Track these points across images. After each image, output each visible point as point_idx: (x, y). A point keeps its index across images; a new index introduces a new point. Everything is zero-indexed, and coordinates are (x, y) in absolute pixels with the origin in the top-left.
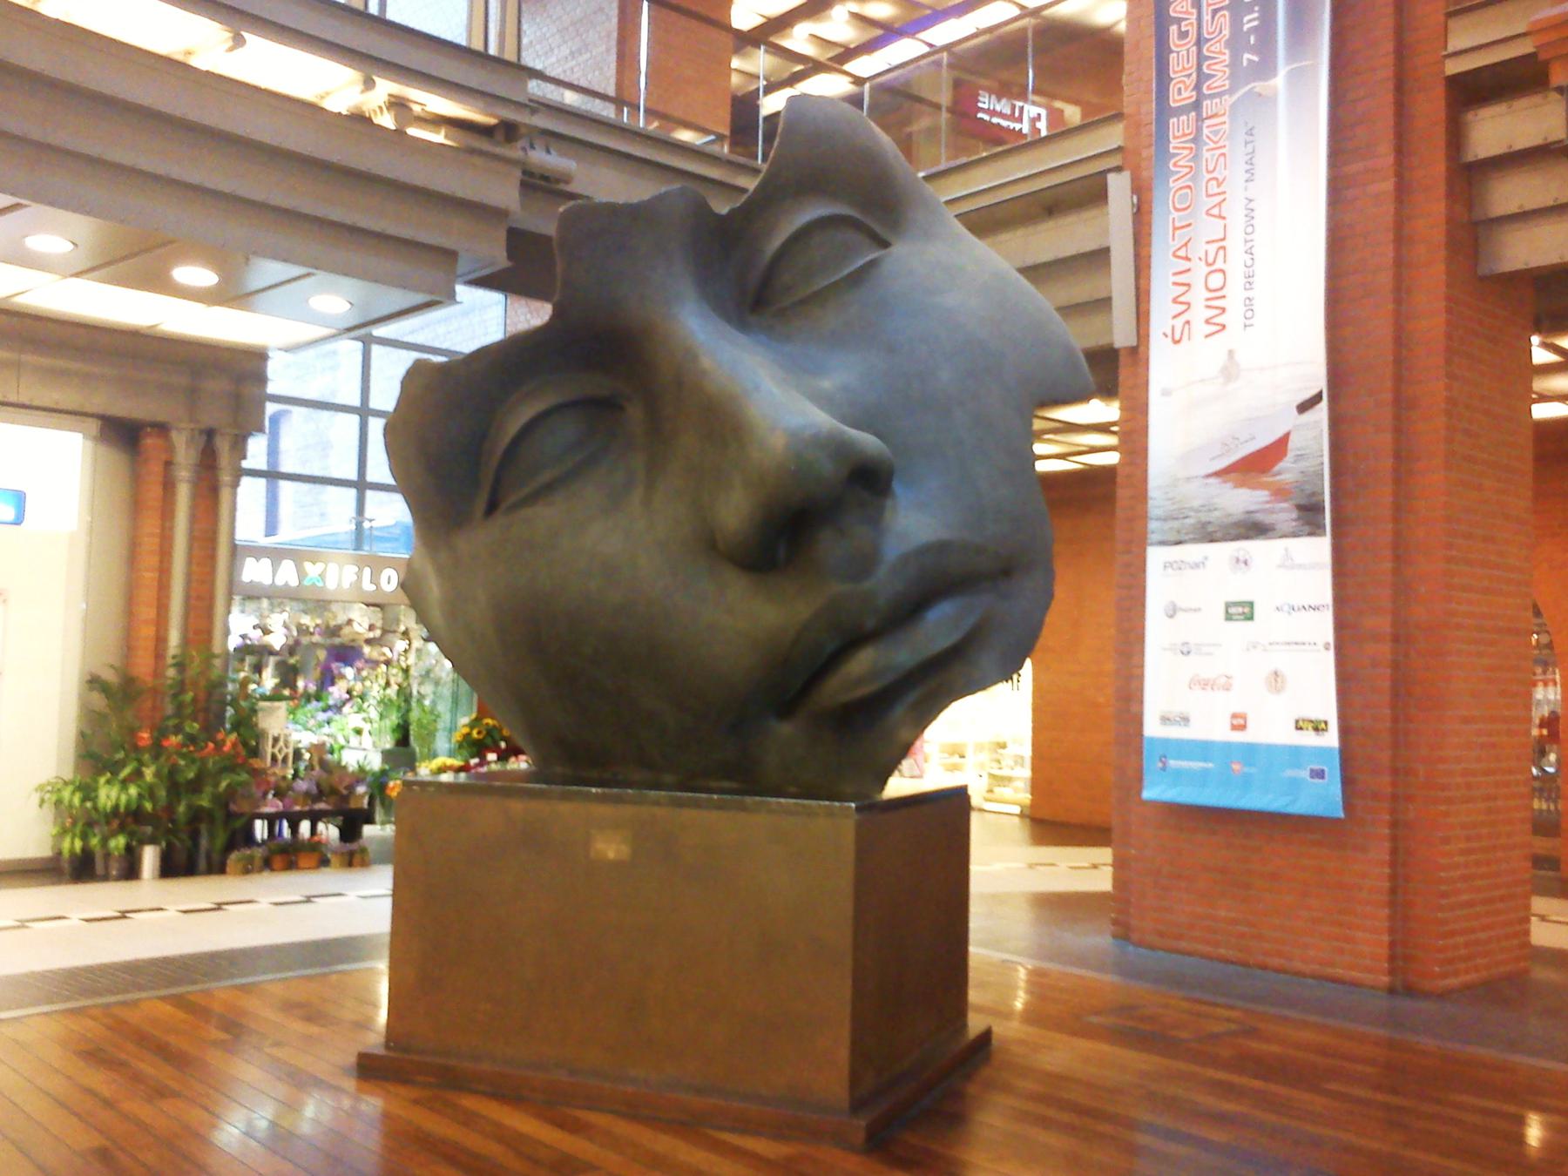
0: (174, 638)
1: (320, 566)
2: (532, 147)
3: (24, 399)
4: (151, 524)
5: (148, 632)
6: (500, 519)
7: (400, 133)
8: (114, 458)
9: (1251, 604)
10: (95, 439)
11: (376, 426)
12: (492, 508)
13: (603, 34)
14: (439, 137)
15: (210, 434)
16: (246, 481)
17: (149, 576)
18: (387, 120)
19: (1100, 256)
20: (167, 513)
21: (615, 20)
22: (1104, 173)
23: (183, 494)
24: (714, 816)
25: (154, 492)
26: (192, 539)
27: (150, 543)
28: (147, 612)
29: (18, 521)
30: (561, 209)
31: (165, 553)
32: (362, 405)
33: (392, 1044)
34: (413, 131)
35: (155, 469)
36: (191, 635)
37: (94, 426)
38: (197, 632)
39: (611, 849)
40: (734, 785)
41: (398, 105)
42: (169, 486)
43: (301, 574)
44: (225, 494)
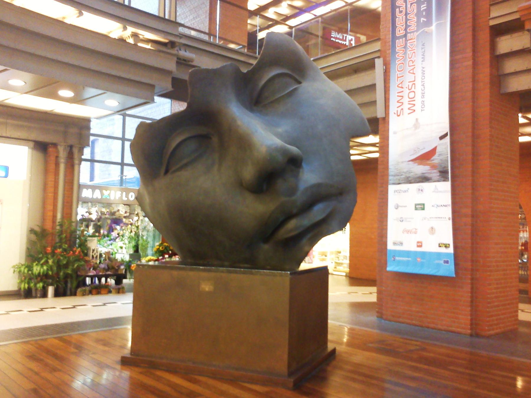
0: (59, 216)
1: (108, 192)
2: (180, 50)
3: (8, 135)
4: (51, 177)
5: (50, 214)
6: (169, 176)
7: (135, 45)
8: (39, 155)
9: (424, 205)
10: (32, 148)
11: (127, 144)
12: (167, 172)
13: (204, 11)
14: (149, 46)
15: (71, 147)
16: (83, 163)
17: (51, 195)
18: (131, 41)
19: (373, 87)
20: (57, 173)
21: (208, 7)
22: (374, 59)
23: (62, 167)
24: (242, 276)
25: (52, 166)
26: (65, 182)
27: (51, 184)
28: (50, 207)
29: (6, 176)
30: (190, 71)
31: (56, 187)
32: (122, 137)
33: (133, 353)
34: (140, 44)
35: (52, 159)
36: (65, 215)
37: (32, 144)
38: (67, 214)
39: (207, 287)
40: (249, 266)
41: (135, 35)
42: (57, 164)
43: (102, 194)
44: (76, 167)
